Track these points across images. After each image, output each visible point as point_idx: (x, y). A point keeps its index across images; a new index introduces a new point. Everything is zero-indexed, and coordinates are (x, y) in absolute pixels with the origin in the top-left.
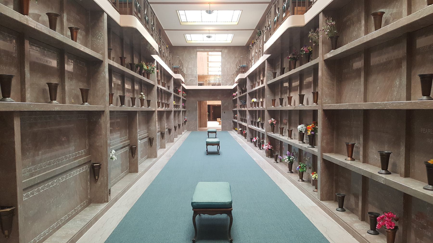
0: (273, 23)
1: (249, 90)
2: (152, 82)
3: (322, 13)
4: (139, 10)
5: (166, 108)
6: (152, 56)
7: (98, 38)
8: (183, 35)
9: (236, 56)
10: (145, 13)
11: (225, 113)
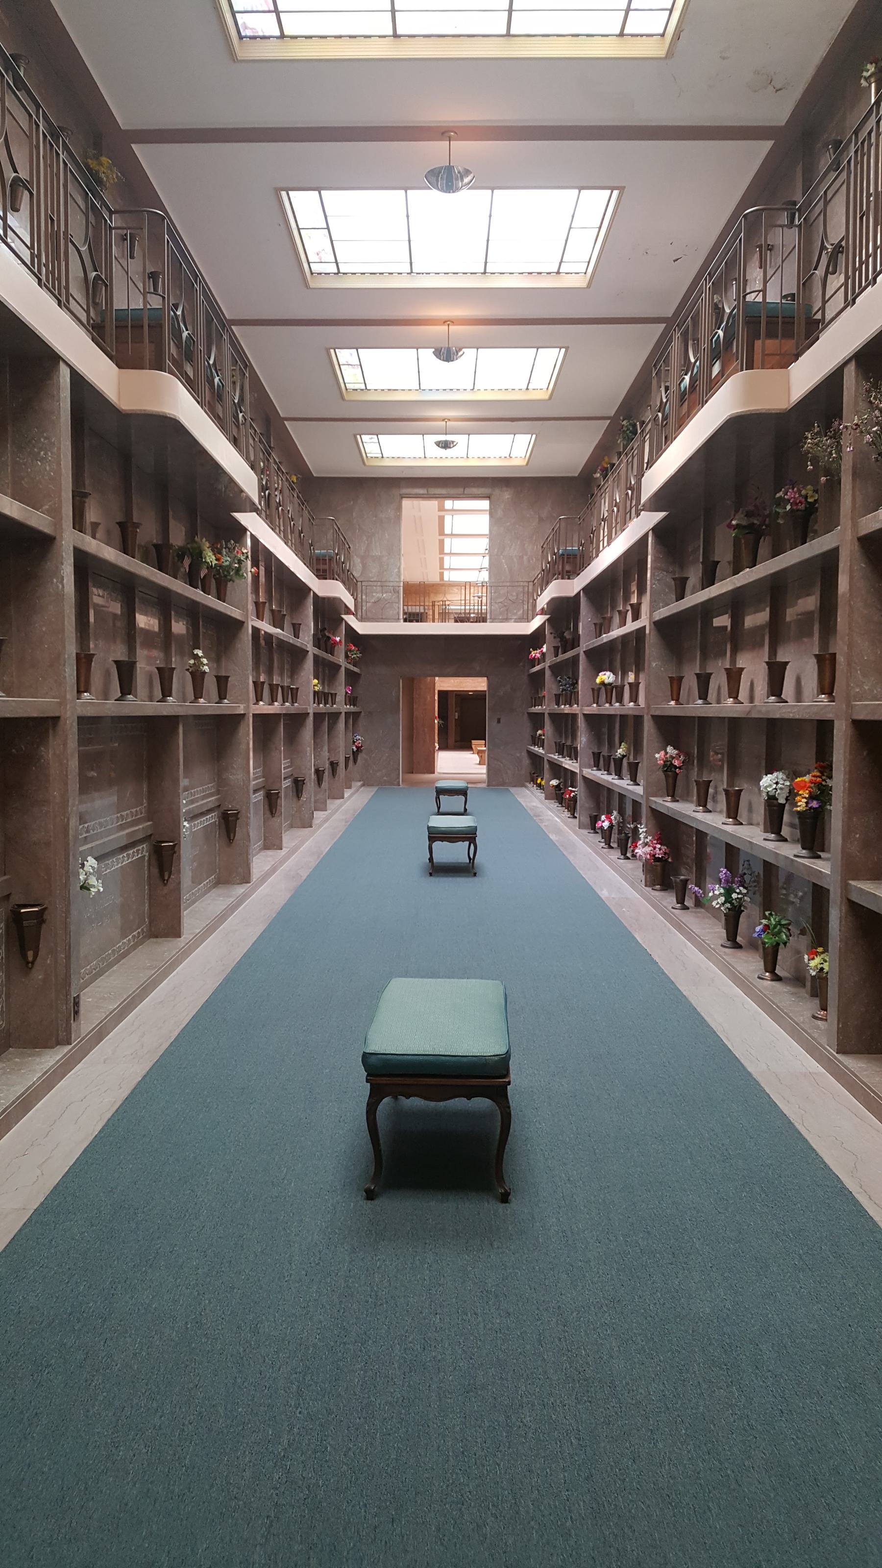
0: (675, 399)
1: (587, 642)
2: (235, 613)
3: (853, 363)
4: (188, 353)
5: (287, 704)
6: (237, 515)
7: (39, 453)
8: (353, 438)
9: (544, 513)
10: (211, 362)
11: (499, 721)
